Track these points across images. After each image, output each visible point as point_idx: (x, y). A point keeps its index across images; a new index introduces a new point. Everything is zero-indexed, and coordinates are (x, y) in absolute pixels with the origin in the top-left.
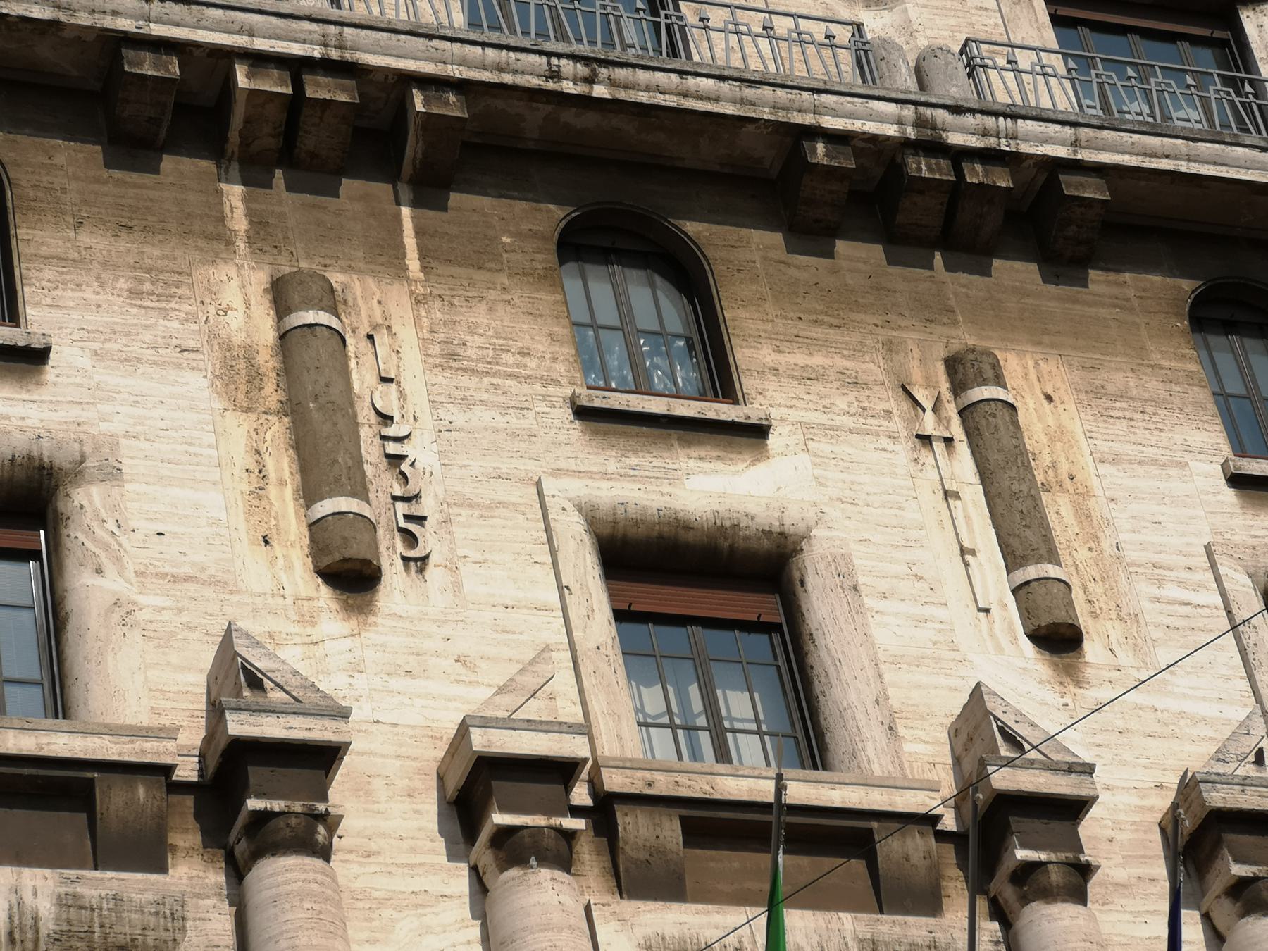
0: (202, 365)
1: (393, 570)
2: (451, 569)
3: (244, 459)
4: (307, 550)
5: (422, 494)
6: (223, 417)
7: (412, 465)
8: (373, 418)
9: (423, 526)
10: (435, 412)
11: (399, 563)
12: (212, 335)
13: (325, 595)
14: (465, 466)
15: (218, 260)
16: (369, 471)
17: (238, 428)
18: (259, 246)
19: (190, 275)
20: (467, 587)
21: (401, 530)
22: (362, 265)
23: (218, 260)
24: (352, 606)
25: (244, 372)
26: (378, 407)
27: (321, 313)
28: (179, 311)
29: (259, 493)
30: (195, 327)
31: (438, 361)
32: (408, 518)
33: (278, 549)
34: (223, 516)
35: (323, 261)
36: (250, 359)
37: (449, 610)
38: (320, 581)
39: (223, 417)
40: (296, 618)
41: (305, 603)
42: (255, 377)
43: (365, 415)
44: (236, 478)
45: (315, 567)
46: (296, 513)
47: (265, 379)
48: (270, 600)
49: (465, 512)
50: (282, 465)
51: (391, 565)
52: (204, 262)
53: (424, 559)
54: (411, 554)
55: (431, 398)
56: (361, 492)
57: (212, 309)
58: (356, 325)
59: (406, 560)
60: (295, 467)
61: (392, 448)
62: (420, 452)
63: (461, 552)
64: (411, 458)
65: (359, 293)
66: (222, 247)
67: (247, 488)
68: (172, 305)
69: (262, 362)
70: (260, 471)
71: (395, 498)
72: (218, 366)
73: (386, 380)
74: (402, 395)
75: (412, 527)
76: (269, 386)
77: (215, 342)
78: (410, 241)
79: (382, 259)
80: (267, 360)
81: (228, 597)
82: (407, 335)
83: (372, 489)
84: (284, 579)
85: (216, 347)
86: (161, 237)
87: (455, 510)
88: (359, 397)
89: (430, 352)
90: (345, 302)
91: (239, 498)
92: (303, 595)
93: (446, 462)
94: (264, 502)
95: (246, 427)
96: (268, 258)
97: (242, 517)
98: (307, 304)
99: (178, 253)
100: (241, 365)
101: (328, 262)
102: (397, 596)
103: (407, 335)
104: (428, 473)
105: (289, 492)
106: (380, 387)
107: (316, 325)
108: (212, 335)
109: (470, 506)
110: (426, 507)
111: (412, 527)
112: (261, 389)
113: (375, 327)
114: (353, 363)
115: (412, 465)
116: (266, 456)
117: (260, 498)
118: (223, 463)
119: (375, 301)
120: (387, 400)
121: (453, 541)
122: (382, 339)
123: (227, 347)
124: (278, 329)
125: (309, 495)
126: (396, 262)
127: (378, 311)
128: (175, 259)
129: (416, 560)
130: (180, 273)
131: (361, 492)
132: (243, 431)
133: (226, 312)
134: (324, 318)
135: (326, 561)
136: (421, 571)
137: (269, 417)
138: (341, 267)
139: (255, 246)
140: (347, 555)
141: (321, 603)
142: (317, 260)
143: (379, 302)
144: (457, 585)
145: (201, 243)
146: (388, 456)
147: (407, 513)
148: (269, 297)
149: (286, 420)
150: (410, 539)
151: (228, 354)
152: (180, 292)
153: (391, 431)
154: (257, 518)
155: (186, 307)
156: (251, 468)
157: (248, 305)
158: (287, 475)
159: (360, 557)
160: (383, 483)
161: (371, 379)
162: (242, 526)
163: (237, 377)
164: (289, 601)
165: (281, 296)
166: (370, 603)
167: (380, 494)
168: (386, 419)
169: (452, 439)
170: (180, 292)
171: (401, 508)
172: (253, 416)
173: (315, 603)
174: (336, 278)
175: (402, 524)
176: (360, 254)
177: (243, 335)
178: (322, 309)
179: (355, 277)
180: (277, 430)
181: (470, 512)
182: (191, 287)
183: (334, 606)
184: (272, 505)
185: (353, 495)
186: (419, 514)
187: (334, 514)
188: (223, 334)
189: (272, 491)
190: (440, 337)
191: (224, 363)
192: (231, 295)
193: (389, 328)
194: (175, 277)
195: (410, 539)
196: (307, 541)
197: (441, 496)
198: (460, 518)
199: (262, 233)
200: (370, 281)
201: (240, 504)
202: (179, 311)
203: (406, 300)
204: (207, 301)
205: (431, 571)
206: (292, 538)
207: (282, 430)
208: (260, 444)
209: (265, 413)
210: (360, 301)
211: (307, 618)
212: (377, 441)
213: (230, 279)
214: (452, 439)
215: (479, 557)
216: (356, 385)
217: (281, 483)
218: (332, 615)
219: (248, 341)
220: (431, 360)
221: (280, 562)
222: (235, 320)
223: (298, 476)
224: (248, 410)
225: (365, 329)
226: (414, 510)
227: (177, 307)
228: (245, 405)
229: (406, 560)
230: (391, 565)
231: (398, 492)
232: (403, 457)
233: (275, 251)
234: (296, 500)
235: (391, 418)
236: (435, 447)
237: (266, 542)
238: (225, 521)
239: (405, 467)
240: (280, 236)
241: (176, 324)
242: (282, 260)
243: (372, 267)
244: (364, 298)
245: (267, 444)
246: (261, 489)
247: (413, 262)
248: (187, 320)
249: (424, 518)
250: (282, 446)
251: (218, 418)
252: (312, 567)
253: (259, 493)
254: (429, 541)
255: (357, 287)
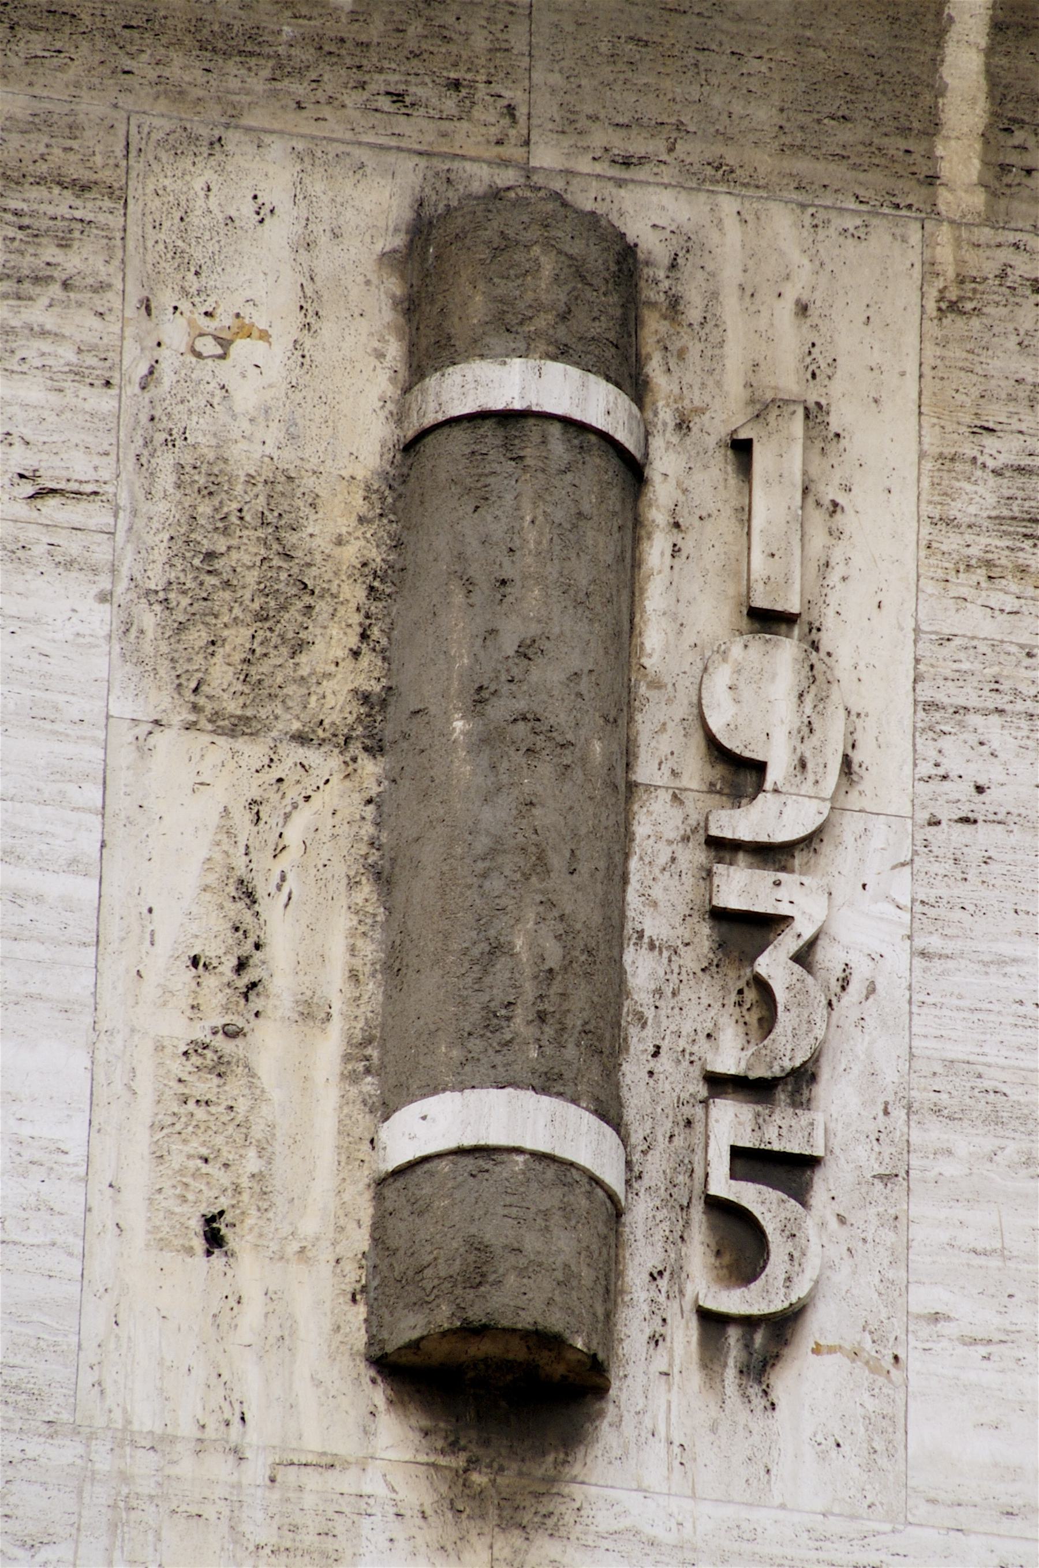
0: (102, 554)
1: (660, 1363)
2: (874, 1367)
3: (187, 915)
4: (353, 1275)
5: (825, 1074)
6: (143, 749)
7: (804, 957)
8: (695, 770)
9: (801, 1194)
10: (928, 748)
11: (685, 1336)
12: (159, 434)
13: (389, 1450)
14: (1001, 961)
15: (232, 137)
16: (642, 970)
17: (191, 795)
18: (394, 80)
19: (119, 195)
20: (925, 1432)
21: (717, 1206)
22: (764, 161)
23: (232, 137)
24: (479, 1496)
25: (251, 578)
26: (716, 725)
27: (556, 370)
28: (57, 336)
29: (216, 1055)
30: (104, 402)
31: (978, 545)
32: (748, 1161)
33: (248, 1265)
34: (73, 1135)
35: (621, 144)
36: (277, 528)
37: (835, 1526)
38: (379, 1395)
39: (143, 749)
40: (266, 1535)
41: (312, 1479)
42: (287, 598)
43: (666, 757)
44: (150, 989)
45: (372, 1341)
46: (343, 1131)
47: (323, 608)
48: (186, 1466)
49: (967, 1142)
50: (320, 942)
51: (655, 1340)
52: (183, 143)
53: (782, 1327)
54: (733, 1301)
55: (926, 692)
56: (587, 1061)
57: (175, 332)
58: (696, 397)
59: (712, 1322)
60: (370, 950)
61: (741, 888)
62: (850, 909)
63: (923, 1298)
64: (804, 928)
65: (730, 274)
66: (258, 84)
67: (181, 1031)
68: (36, 314)
69: (323, 543)
70: (241, 966)
71: (719, 1084)
72: (160, 555)
73: (767, 621)
74: (815, 680)
75: (749, 1195)
76: (333, 639)
77: (165, 461)
78: (964, 65)
79: (845, 134)
80: (338, 535)
81: (34, 1448)
82: (885, 441)
83: (639, 1042)
84: (252, 1384)
85: (167, 480)
86: (37, 43)
87: (930, 1134)
88: (656, 685)
89: (954, 510)
90: (674, 305)
91: (146, 1064)
92: (313, 1442)
93: (935, 943)
94: (235, 1086)
95: (219, 795)
96: (417, 130)
97: (142, 1141)
98: (512, 331)
99: (93, 107)
100: (244, 554)
101: (638, 145)
102: (654, 1464)
103: (885, 441)
104: (856, 987)
105: (329, 1048)
106: (736, 650)
107: (526, 414)
108: (159, 434)
109: (994, 1120)
110: (835, 1122)
111: (749, 1195)
112: (299, 647)
113: (764, 408)
114: (656, 552)
115: (804, 957)
116: (271, 908)
117: (220, 1069)
118: (113, 931)
119: (786, 308)
120: (756, 700)
121: (902, 1255)
122: (780, 457)
123: (208, 480)
124: (400, 418)
125: (391, 1069)
126: (896, 144)
127: (789, 338)
128: (74, 130)
129: (749, 1322)
130: (83, 188)
131: (587, 1061)
132: (206, 810)
133: (225, 344)
134: (587, 397)
135: (408, 1327)
136: (759, 1369)
137: (311, 756)
138: (685, 168)
139: (378, 83)
140: (476, 1314)
141: (373, 1484)
142: (600, 137)
143: (803, 309)
144: (887, 1433)
145: (183, 68)
146: (720, 916)
147: (747, 1141)
148: (394, 286)
149: (370, 768)
150: (743, 1247)
151: (205, 508)
152: (71, 262)
153: (745, 823)
154: (195, 1146)
155: (81, 325)
156: (210, 951)
157: (309, 312)
158: (334, 986)
159: (525, 1321)
160: (681, 1021)
161: (712, 614)
162: (138, 1176)
163: (221, 595)
164: (256, 1469)
165: (441, 281)
166: (548, 1488)
167: (664, 1063)
168: (740, 773)
169: (974, 855)
170: (71, 262)
171: (731, 1123)
172: (253, 752)
173: (345, 1482)
174: (650, 214)
175: (722, 1186)
176: (764, 114)
177: (274, 434)
178: (562, 353)
179: (728, 205)
180: (330, 805)
181: (989, 1144)
182: (115, 243)
183: (416, 1493)
184: (258, 1097)
185: (547, 1083)
186: (794, 1147)
187: (461, 1152)
188: (201, 432)
189: (270, 1044)
190: (1002, 450)
191: (184, 542)
192: (258, 280)
193: (814, 414)
194: (62, 204)
195: (743, 1247)
196: (360, 1240)
197: (890, 1076)
198: (949, 1168)
199: (415, 28)
200: (782, 223)
201: (145, 1086)
202: (57, 336)
203: (905, 299)
204: (165, 298)
205: (806, 1378)
206: (310, 1226)
207: (352, 805)
208: (262, 860)
209: (301, 739)
210: (730, 306)
211: (308, 1539)
212: (695, 855)
213: (263, 214)
214: (974, 855)
215: (986, 1319)
216: (654, 638)
217: (310, 1013)
218: (398, 1531)
219: (287, 458)
220: (951, 542)
221: (252, 1314)
222: (256, 375)
223: (372, 988)
224: (239, 727)
225: (726, 415)
226: (783, 1132)
227: (49, 320)
228: (233, 707)
229: (712, 1322)
230: (655, 1340)
231: (729, 1061)
232: (765, 925)
233: (450, 104)
234: (352, 1078)
235: (760, 768)
236: (902, 887)
237: (214, 1240)
238: (77, 1153)
239: (774, 963)
240: (480, 42)
241: (33, 391)
242: (470, 137)
243: (802, 165)
244: (748, 293)
245: (285, 862)
246: (232, 1033)
247: (960, 158)
248: (77, 373)
249: (810, 1162)
250: (339, 869)
251: (124, 756)
252: (360, 1339)
253: (216, 1055)
254: (815, 1250)
255: (729, 244)
